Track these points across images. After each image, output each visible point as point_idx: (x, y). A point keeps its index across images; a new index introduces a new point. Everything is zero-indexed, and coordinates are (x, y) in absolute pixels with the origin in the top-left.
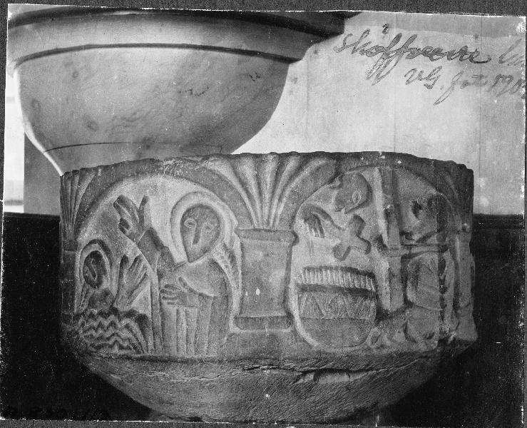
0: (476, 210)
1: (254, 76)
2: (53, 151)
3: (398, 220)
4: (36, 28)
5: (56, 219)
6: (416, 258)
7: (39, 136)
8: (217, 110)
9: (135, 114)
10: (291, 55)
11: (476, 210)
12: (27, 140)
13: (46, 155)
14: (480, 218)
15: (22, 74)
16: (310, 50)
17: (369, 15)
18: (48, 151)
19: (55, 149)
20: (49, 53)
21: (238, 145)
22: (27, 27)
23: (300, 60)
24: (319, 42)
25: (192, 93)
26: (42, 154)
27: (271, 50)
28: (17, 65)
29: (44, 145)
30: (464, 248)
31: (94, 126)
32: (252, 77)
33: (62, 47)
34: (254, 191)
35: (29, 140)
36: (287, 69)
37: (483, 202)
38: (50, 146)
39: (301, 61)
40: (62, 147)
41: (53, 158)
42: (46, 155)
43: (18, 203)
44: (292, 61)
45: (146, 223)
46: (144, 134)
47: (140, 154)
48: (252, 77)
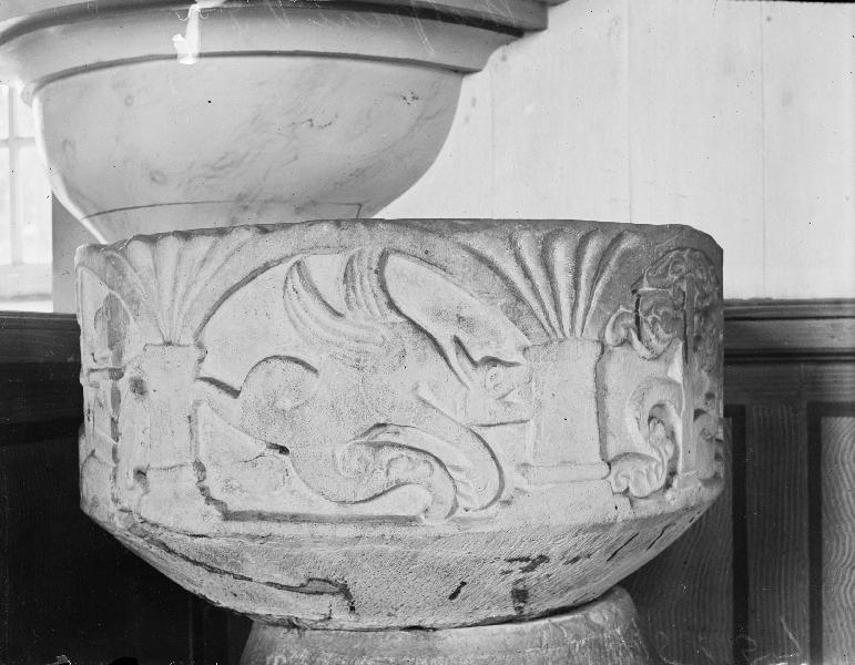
0: (727, 295)
1: (409, 97)
4: (64, 32)
5: (66, 330)
6: (124, 260)
7: (73, 191)
11: (727, 295)
12: (56, 204)
13: (87, 224)
14: (730, 303)
15: (45, 104)
16: (496, 55)
19: (522, 422)
22: (52, 30)
23: (479, 70)
25: (312, 125)
27: (432, 55)
28: (39, 88)
29: (83, 209)
34: (181, 289)
36: (459, 90)
37: (739, 284)
39: (479, 74)
41: (98, 229)
42: (87, 224)
43: (42, 297)
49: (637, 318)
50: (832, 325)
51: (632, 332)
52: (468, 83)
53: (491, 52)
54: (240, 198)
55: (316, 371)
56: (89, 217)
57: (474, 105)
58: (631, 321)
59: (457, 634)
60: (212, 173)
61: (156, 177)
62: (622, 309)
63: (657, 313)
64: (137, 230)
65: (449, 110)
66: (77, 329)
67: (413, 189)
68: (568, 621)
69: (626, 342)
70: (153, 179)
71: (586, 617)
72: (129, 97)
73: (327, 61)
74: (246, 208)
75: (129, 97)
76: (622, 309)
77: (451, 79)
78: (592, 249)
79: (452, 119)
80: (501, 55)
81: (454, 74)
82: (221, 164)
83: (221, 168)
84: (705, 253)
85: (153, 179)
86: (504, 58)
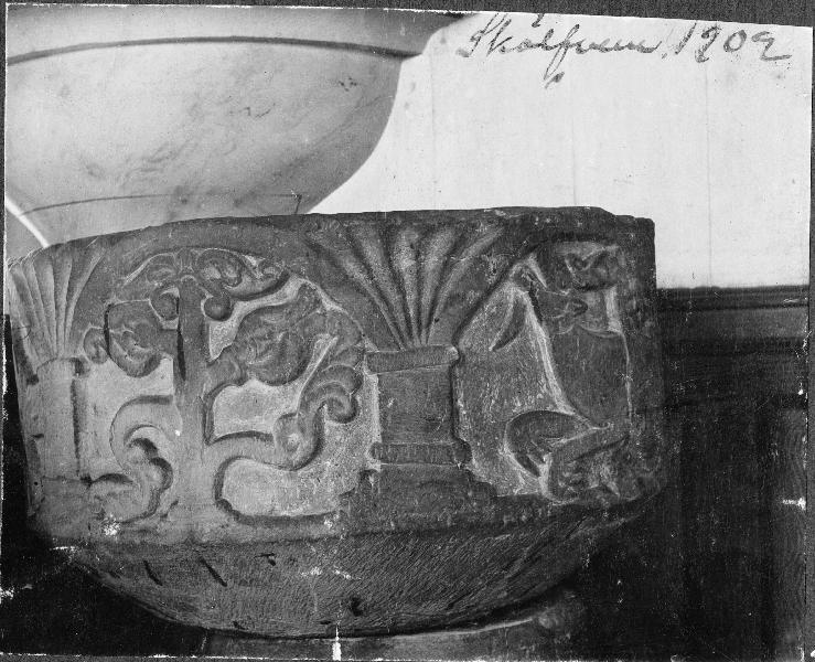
1: (347, 82)
2: (34, 213)
8: (305, 138)
9: (160, 150)
10: (404, 48)
11: (659, 285)
13: (24, 220)
16: (435, 38)
17: (120, 8)
18: (26, 213)
20: (74, 49)
25: (249, 114)
26: (18, 220)
31: (96, 171)
32: (343, 84)
33: (60, 46)
37: (677, 268)
38: (29, 207)
39: (417, 58)
40: (48, 207)
41: (35, 224)
42: (24, 220)
44: (403, 56)
45: (295, 276)
46: (177, 182)
47: (173, 215)
48: (343, 84)
49: (106, 333)
50: (782, 314)
51: (101, 349)
52: (407, 67)
54: (178, 191)
56: (27, 213)
58: (101, 338)
59: (405, 641)
60: (150, 166)
61: (92, 171)
62: (90, 326)
63: (127, 326)
64: (74, 226)
67: (356, 176)
68: (518, 626)
69: (96, 358)
70: (91, 173)
71: (536, 620)
72: (65, 87)
73: (264, 47)
74: (185, 201)
75: (65, 87)
76: (90, 326)
77: (386, 64)
78: (440, 243)
80: (440, 37)
82: (160, 155)
83: (160, 160)
85: (91, 173)
86: (443, 41)
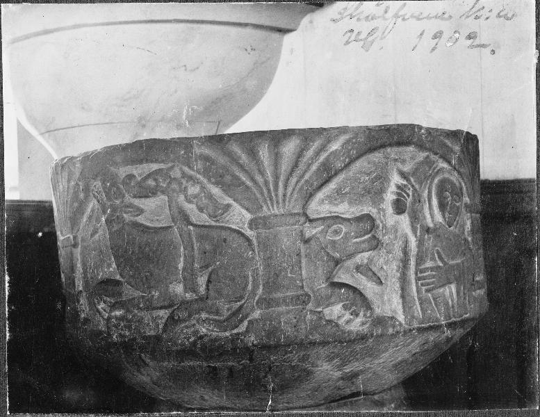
0: (482, 177)
2: (47, 135)
3: (89, 189)
9: (129, 93)
11: (482, 177)
12: (19, 124)
13: (40, 139)
14: (482, 180)
16: (306, 20)
21: (237, 118)
23: (296, 30)
24: (313, 11)
25: (186, 70)
30: (286, 17)
32: (246, 50)
35: (23, 128)
37: (492, 167)
38: (43, 130)
39: (295, 32)
42: (40, 139)
48: (246, 50)
52: (288, 38)
53: (302, 18)
54: (140, 119)
55: (424, 31)
56: (42, 134)
57: (292, 49)
65: (276, 52)
66: (52, 210)
70: (83, 108)
73: (195, 26)
77: (276, 35)
79: (248, 112)
80: (309, 20)
81: (278, 33)
84: (470, 143)
85: (83, 108)
86: (311, 22)
